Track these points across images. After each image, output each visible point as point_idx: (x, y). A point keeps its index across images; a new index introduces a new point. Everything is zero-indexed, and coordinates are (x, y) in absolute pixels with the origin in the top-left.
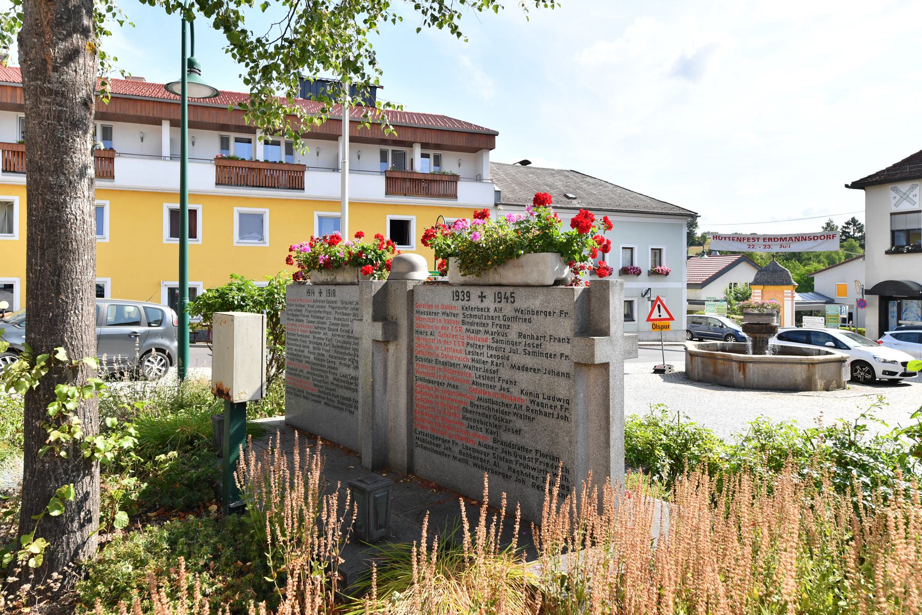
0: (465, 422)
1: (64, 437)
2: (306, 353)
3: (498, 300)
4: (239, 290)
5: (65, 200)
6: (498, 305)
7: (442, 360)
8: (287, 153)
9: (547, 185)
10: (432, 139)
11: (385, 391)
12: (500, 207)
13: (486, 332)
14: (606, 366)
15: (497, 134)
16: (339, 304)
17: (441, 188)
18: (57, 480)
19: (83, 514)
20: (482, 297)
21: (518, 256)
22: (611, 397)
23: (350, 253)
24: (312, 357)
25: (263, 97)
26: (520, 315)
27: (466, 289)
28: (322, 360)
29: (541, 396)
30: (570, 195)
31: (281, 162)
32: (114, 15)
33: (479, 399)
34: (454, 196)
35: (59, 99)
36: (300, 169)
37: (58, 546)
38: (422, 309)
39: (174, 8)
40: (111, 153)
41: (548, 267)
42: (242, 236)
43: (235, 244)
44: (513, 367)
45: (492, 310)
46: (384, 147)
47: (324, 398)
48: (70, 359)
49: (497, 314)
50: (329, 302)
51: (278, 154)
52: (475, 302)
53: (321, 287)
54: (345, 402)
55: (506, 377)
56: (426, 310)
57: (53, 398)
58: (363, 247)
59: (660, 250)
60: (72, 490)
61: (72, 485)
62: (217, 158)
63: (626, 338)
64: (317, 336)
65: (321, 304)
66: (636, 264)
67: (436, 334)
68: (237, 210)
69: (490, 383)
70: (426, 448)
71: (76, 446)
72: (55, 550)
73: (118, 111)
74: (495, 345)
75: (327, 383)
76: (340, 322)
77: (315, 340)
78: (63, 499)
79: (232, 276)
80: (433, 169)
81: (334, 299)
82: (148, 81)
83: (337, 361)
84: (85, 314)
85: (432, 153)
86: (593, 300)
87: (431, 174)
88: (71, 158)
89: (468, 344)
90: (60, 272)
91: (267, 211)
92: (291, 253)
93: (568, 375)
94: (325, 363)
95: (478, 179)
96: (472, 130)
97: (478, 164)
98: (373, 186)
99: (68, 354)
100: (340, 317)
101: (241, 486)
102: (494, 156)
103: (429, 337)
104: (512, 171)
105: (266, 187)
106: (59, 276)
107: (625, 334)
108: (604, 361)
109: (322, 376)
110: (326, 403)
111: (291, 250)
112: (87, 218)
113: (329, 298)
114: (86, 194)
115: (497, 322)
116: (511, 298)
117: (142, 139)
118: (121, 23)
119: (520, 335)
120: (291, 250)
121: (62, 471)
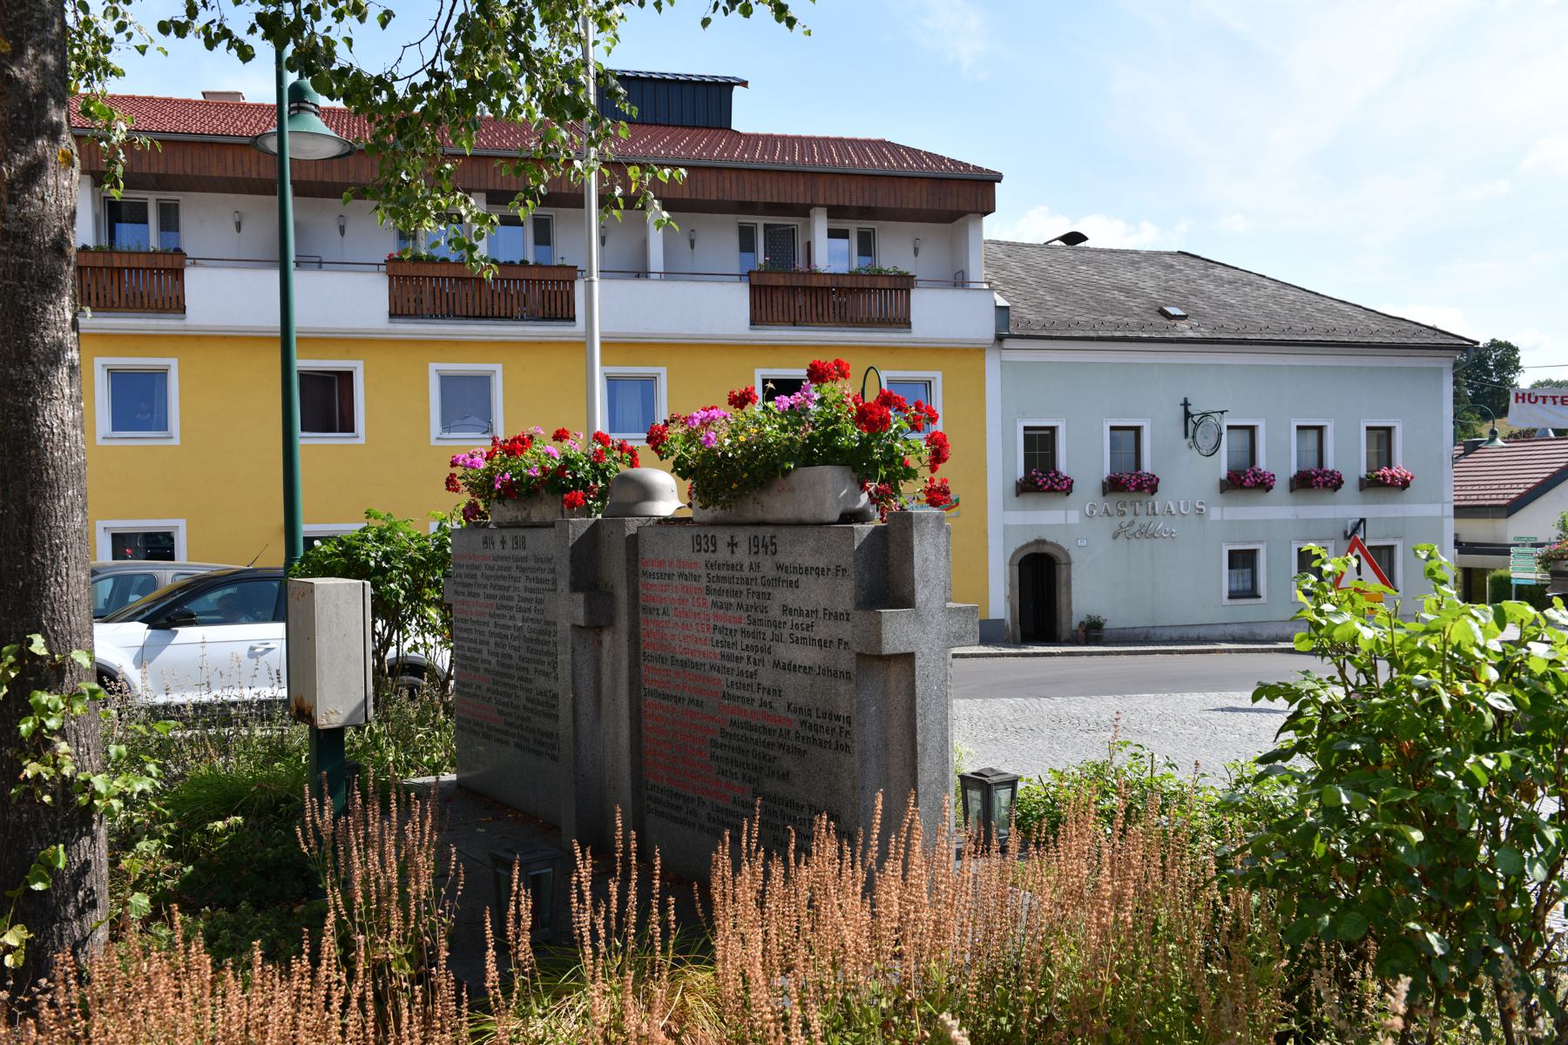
0: (713, 764)
1: (47, 773)
2: (485, 655)
3: (754, 549)
4: (381, 538)
5: (34, 403)
6: (753, 559)
7: (679, 657)
8: (537, 242)
9: (1121, 290)
10: (854, 196)
11: (598, 716)
12: (1008, 343)
13: (740, 606)
14: (909, 658)
15: (998, 178)
16: (531, 563)
17: (874, 305)
18: (40, 840)
19: (81, 893)
20: (732, 545)
21: (787, 472)
22: (919, 711)
23: (543, 468)
24: (494, 661)
25: (403, 176)
26: (784, 576)
27: (711, 532)
28: (509, 666)
29: (814, 714)
30: (1173, 311)
31: (524, 263)
32: (129, 36)
33: (733, 723)
34: (904, 323)
35: (19, 245)
36: (565, 275)
37: (46, 939)
38: (650, 569)
39: (219, 38)
40: (177, 258)
41: (829, 490)
42: (447, 425)
43: (433, 442)
44: (776, 664)
45: (746, 566)
46: (747, 219)
47: (513, 735)
48: (50, 651)
49: (752, 575)
50: (517, 559)
51: (519, 246)
52: (723, 554)
53: (504, 532)
54: (545, 739)
55: (766, 683)
56: (656, 570)
57: (29, 711)
58: (566, 458)
59: (1389, 430)
60: (61, 853)
61: (61, 846)
62: (391, 261)
63: (951, 610)
64: (501, 622)
65: (504, 563)
66: (1330, 465)
67: (671, 612)
68: (435, 370)
69: (747, 694)
70: (661, 814)
71: (66, 788)
72: (41, 946)
73: (189, 171)
74: (751, 628)
75: (517, 707)
76: (533, 596)
77: (498, 630)
78: (50, 868)
79: (368, 514)
80: (856, 263)
81: (523, 553)
82: (248, 100)
83: (531, 667)
84: (73, 583)
85: (853, 226)
86: (892, 546)
87: (851, 274)
88: (42, 337)
89: (715, 627)
90: (31, 518)
91: (498, 368)
92: (454, 470)
93: (847, 676)
94: (513, 672)
95: (959, 281)
96: (943, 171)
97: (958, 247)
98: (722, 307)
99: (48, 645)
100: (534, 585)
101: (310, 850)
102: (993, 228)
103: (661, 618)
104: (1041, 261)
105: (493, 317)
106: (30, 524)
107: (950, 605)
108: (902, 649)
109: (509, 696)
110: (517, 745)
111: (453, 464)
112: (69, 430)
113: (516, 553)
114: (67, 391)
115: (754, 588)
116: (770, 547)
117: (239, 226)
118: (142, 50)
119: (786, 610)
120: (453, 464)
121: (46, 826)
